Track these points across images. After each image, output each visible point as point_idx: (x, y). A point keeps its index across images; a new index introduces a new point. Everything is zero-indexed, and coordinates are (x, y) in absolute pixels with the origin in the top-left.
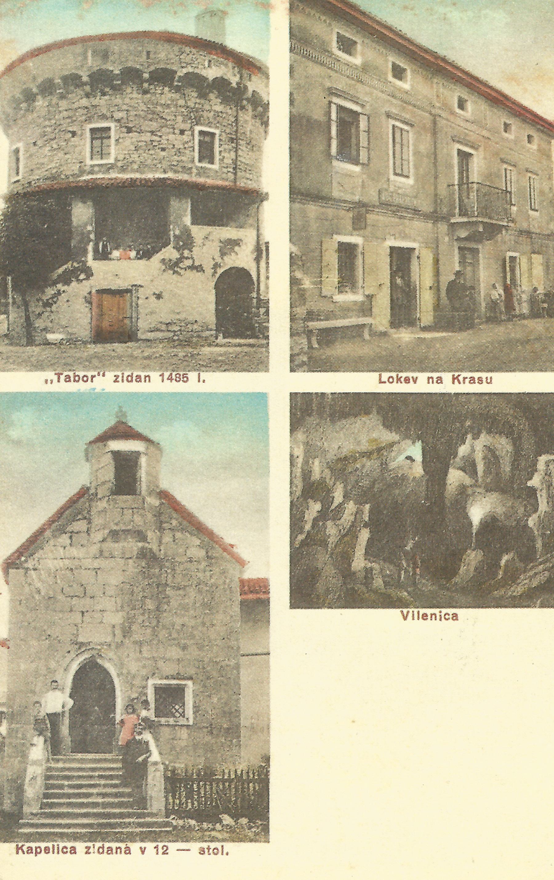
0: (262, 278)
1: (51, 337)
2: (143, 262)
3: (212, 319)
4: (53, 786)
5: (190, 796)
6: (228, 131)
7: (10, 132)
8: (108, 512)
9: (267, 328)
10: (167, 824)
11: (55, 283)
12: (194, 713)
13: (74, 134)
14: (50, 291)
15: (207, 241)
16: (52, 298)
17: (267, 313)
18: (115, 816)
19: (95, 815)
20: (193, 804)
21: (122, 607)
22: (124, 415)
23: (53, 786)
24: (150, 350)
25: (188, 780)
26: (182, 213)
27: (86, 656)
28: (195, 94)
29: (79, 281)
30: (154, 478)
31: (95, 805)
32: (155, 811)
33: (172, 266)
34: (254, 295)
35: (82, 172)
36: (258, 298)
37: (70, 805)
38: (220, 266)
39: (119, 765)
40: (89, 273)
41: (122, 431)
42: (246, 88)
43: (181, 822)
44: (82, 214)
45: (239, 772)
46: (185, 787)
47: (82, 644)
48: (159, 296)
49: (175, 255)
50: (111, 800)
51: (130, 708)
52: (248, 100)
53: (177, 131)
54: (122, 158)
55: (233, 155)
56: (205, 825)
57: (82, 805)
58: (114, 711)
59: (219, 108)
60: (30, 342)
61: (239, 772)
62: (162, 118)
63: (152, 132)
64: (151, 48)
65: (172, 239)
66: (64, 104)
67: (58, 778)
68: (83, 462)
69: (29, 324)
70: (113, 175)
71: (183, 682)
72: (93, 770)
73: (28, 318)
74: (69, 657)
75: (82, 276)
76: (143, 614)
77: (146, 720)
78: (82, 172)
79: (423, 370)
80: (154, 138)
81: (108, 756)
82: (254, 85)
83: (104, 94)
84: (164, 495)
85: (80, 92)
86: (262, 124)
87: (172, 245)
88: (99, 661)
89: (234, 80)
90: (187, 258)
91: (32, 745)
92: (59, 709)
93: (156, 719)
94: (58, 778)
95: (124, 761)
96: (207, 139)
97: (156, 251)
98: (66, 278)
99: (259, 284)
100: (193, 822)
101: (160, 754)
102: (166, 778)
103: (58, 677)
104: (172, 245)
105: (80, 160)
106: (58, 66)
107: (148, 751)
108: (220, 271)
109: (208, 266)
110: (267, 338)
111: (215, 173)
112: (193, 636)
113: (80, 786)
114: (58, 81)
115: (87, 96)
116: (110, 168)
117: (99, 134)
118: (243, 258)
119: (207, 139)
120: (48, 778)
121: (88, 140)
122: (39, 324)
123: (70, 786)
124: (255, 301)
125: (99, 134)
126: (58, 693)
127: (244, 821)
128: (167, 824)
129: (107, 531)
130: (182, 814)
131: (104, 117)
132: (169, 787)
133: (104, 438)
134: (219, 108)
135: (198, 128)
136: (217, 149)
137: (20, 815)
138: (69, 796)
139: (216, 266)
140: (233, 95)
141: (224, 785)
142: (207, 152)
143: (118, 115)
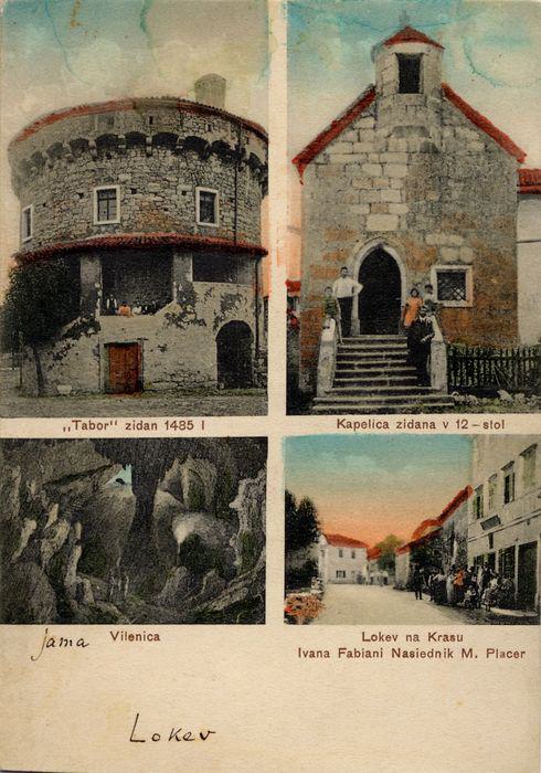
0: (261, 329)
1: (61, 388)
2: (148, 317)
3: (215, 374)
4: (344, 366)
5: (470, 374)
6: (228, 191)
7: (26, 191)
8: (395, 107)
9: (266, 378)
10: (449, 400)
11: (66, 336)
12: (474, 295)
13: (81, 195)
14: (61, 345)
15: (210, 298)
16: (62, 352)
17: (266, 364)
18: (401, 392)
19: (382, 393)
20: (473, 381)
21: (407, 199)
22: (407, 18)
23: (344, 366)
24: (156, 400)
25: (467, 359)
26: (184, 267)
27: (374, 244)
28: (195, 157)
29: (88, 335)
30: (437, 76)
31: (383, 383)
32: (438, 388)
33: (176, 320)
34: (253, 346)
35: (90, 232)
36: (257, 349)
37: (360, 383)
38: (221, 320)
39: (406, 345)
40: (97, 327)
41: (408, 35)
42: (244, 150)
43: (462, 398)
44: (90, 271)
45: (516, 351)
46: (466, 365)
47: (369, 234)
48: (163, 349)
49: (179, 310)
50: (398, 378)
51: (415, 293)
52: (247, 162)
53: (180, 193)
54: (123, 219)
55: (232, 213)
56: (485, 400)
57: (369, 384)
58: (400, 296)
59: (219, 170)
60: (42, 395)
61: (516, 351)
62: (165, 180)
63: (156, 194)
64: (154, 114)
65: (175, 295)
66: (72, 168)
67: (348, 358)
68: (371, 62)
69: (41, 380)
70: (119, 234)
71: (464, 267)
72: (381, 350)
73: (39, 372)
74: (361, 244)
75: (91, 331)
76: (427, 205)
77: (428, 302)
78: (90, 232)
79: (394, 438)
80: (157, 198)
81: (393, 337)
82: (253, 147)
83: (109, 157)
84: (447, 93)
85: (87, 155)
86: (260, 183)
87: (175, 301)
88: (387, 249)
89: (233, 144)
90: (190, 313)
91: (324, 328)
92: (348, 293)
93: (439, 302)
94: (348, 358)
95: (408, 341)
96: (208, 199)
97: (159, 307)
98: (74, 334)
99: (257, 335)
100: (472, 397)
101: (443, 334)
102: (449, 358)
103: (348, 265)
104: (175, 301)
105: (93, 221)
106: (65, 132)
107: (431, 331)
108: (221, 325)
109: (210, 321)
110: (266, 387)
111: (219, 228)
112: (473, 225)
113: (369, 374)
114: (66, 145)
115: (94, 159)
116: (116, 227)
117: (106, 196)
118: (243, 313)
119: (208, 199)
120: (339, 358)
121: (95, 203)
122: (50, 376)
123: (360, 366)
124: (254, 352)
125: (106, 196)
126: (348, 280)
127: (520, 396)
128: (449, 400)
129: (392, 128)
130: (464, 391)
131: (111, 180)
132: (452, 366)
133: (391, 42)
134: (219, 170)
135: (199, 189)
136: (217, 208)
137: (314, 393)
138: (358, 375)
139: (218, 320)
140: (231, 156)
141: (502, 364)
142: (208, 210)
143: (122, 177)
